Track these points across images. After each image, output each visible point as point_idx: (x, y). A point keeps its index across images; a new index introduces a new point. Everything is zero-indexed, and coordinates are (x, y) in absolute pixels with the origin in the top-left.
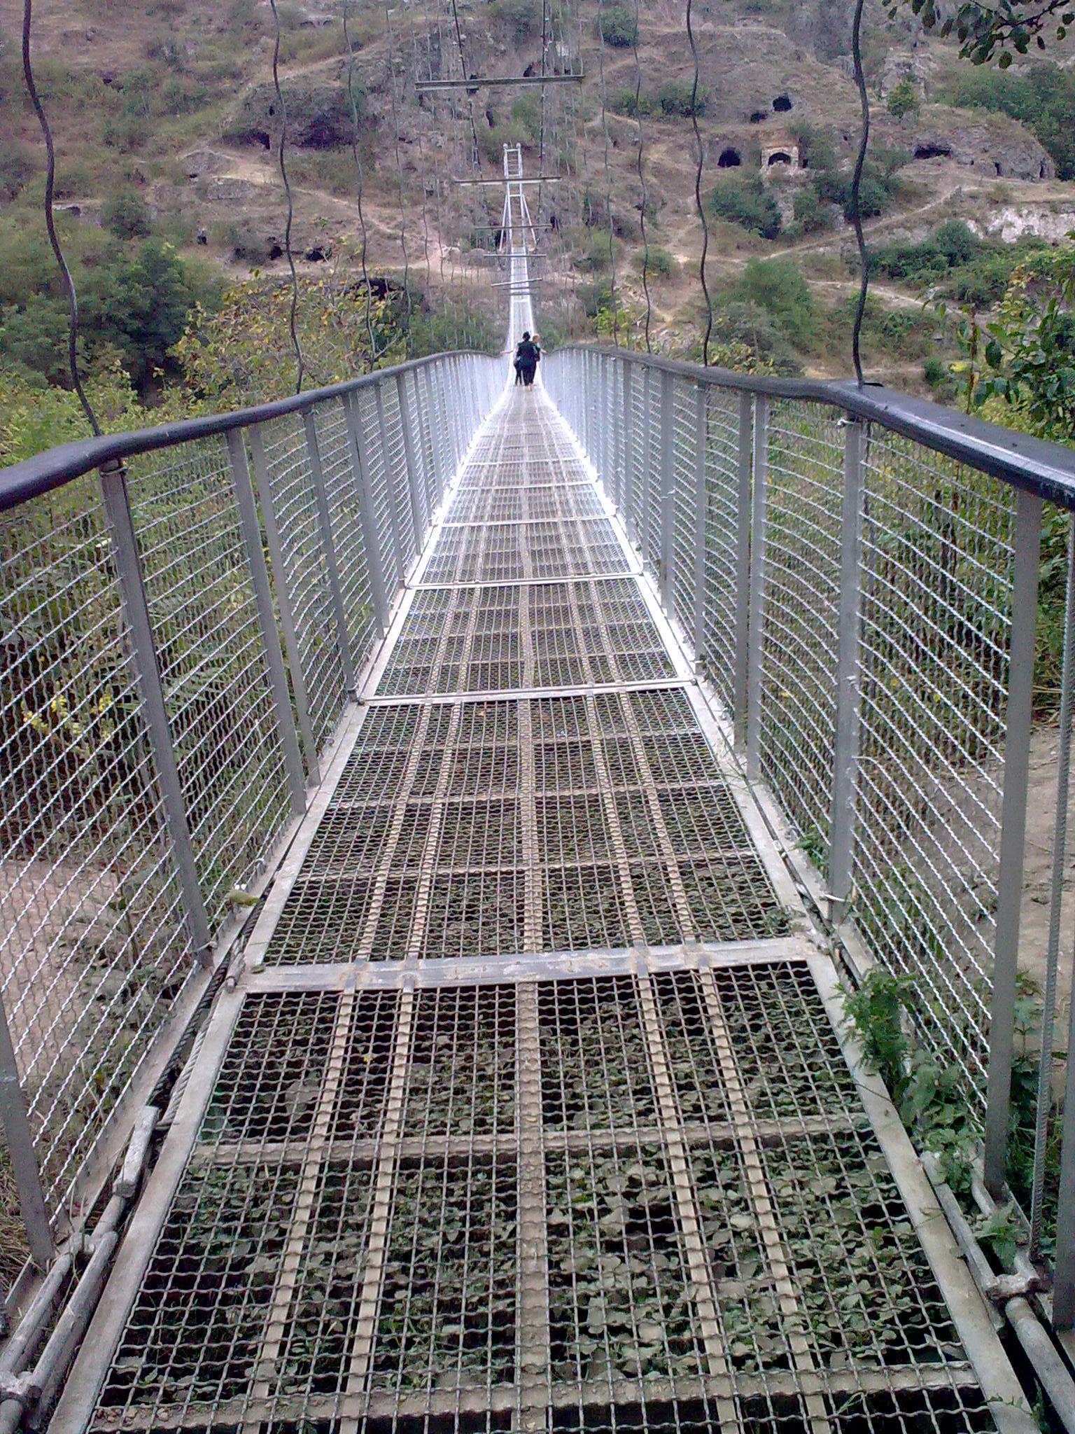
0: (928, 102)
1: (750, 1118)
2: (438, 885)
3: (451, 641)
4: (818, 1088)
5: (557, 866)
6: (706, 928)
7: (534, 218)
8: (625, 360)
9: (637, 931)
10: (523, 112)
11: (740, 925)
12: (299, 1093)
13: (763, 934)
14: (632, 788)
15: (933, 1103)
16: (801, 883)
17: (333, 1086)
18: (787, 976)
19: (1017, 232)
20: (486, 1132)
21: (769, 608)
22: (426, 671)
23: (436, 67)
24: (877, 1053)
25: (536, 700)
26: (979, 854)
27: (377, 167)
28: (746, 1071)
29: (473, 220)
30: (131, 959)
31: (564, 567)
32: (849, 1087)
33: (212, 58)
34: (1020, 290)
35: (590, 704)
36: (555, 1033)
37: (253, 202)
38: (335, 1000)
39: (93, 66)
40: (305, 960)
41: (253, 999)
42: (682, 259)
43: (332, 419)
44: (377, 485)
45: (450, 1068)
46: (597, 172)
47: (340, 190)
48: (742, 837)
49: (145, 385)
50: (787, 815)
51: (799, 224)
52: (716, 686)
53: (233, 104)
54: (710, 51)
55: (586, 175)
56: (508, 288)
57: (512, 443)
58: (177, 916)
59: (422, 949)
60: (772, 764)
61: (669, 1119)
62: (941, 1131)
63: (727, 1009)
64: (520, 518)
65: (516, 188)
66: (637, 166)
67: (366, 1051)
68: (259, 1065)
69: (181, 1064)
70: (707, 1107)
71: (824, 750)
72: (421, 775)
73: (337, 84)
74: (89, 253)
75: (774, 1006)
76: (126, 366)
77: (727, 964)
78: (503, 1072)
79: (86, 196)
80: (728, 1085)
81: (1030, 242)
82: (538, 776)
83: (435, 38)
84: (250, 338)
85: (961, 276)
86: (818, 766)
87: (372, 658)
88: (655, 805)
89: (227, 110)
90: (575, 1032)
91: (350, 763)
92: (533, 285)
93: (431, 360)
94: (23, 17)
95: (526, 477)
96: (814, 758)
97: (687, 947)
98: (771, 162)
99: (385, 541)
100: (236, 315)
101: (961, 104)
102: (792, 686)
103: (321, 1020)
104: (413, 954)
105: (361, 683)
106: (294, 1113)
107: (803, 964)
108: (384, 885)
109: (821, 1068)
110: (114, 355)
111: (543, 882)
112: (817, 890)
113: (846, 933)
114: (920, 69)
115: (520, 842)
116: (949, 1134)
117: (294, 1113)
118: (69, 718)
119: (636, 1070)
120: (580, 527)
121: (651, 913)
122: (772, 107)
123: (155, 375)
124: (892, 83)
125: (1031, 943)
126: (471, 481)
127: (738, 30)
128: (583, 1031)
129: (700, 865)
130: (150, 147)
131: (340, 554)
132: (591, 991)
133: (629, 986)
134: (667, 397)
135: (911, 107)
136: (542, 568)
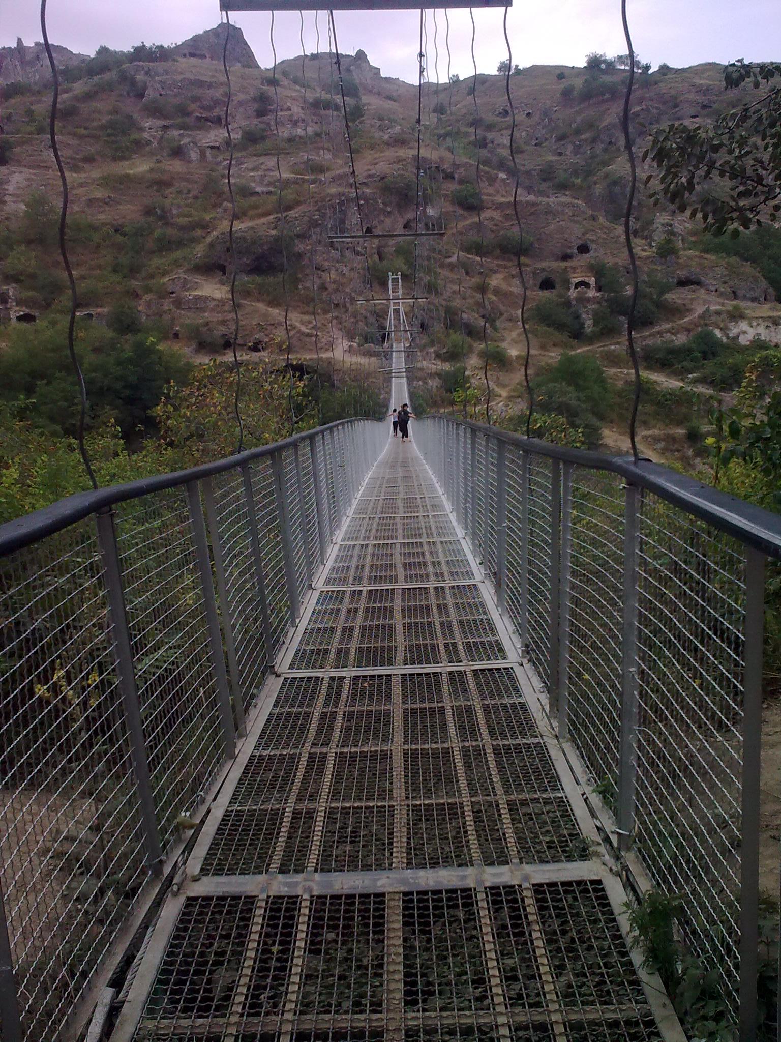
0: (685, 249)
1: (560, 1006)
2: (331, 814)
3: (344, 629)
4: (611, 982)
5: (418, 803)
6: (530, 852)
7: (410, 323)
8: (472, 430)
9: (476, 853)
10: (404, 252)
11: (552, 851)
12: (222, 976)
13: (570, 859)
14: (474, 744)
15: (699, 999)
16: (597, 818)
17: (248, 972)
18: (588, 891)
19: (750, 337)
20: (361, 1012)
21: (573, 614)
22: (326, 651)
23: (343, 221)
24: (656, 958)
25: (405, 675)
26: (727, 802)
27: (300, 287)
28: (556, 967)
29: (367, 325)
30: (102, 871)
31: (427, 575)
32: (636, 983)
33: (189, 216)
34: (751, 381)
35: (445, 678)
36: (414, 933)
37: (212, 310)
38: (252, 903)
39: (108, 221)
40: (231, 872)
41: (191, 901)
42: (514, 352)
43: (264, 468)
44: (293, 509)
45: (336, 958)
46: (454, 292)
47: (273, 303)
48: (555, 782)
49: (131, 439)
50: (588, 767)
51: (597, 329)
52: (536, 667)
53: (201, 245)
54: (532, 214)
55: (447, 294)
56: (390, 372)
57: (392, 484)
58: (137, 837)
59: (317, 864)
60: (576, 728)
61: (499, 1004)
62: (706, 1023)
63: (542, 917)
64: (397, 539)
65: (398, 303)
66: (482, 289)
67: (274, 944)
68: (193, 954)
69: (135, 952)
70: (528, 996)
71: (613, 720)
72: (319, 731)
73: (274, 232)
74: (97, 344)
75: (578, 915)
76: (118, 422)
77: (543, 881)
78: (375, 963)
79: (97, 306)
80: (544, 978)
81: (759, 345)
82: (406, 736)
83: (342, 203)
84: (207, 405)
85: (710, 366)
86: (610, 732)
87: (287, 641)
88: (491, 757)
89: (197, 250)
90: (429, 932)
91: (268, 721)
92: (408, 370)
93: (335, 426)
94: (62, 189)
95: (401, 509)
96: (605, 725)
97: (513, 867)
98: (576, 288)
99: (299, 556)
100: (198, 389)
101: (707, 251)
102: (591, 672)
103: (241, 919)
104: (311, 867)
105: (278, 660)
106: (218, 993)
107: (599, 882)
108: (290, 814)
109: (613, 967)
110: (110, 415)
111: (408, 815)
112: (609, 825)
113: (630, 858)
114: (679, 228)
115: (391, 783)
116: (711, 1025)
117: (218, 993)
118: (68, 689)
119: (475, 964)
120: (439, 546)
121: (487, 840)
122: (576, 251)
123: (137, 429)
124: (659, 237)
125: (771, 870)
126: (361, 510)
127: (553, 199)
128: (435, 930)
129: (524, 803)
130: (144, 274)
131: (266, 565)
132: (441, 900)
133: (470, 897)
134: (501, 458)
135: (673, 253)
136: (411, 576)
